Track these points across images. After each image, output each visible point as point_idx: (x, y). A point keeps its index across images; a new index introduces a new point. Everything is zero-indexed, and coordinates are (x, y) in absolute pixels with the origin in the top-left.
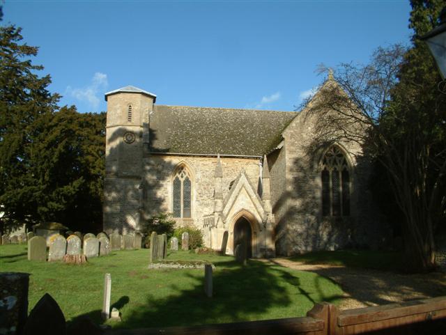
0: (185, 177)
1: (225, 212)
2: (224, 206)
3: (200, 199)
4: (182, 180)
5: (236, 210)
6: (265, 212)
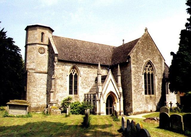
0: (75, 73)
1: (103, 93)
2: (103, 90)
3: (82, 85)
4: (74, 75)
5: (108, 92)
6: (120, 93)
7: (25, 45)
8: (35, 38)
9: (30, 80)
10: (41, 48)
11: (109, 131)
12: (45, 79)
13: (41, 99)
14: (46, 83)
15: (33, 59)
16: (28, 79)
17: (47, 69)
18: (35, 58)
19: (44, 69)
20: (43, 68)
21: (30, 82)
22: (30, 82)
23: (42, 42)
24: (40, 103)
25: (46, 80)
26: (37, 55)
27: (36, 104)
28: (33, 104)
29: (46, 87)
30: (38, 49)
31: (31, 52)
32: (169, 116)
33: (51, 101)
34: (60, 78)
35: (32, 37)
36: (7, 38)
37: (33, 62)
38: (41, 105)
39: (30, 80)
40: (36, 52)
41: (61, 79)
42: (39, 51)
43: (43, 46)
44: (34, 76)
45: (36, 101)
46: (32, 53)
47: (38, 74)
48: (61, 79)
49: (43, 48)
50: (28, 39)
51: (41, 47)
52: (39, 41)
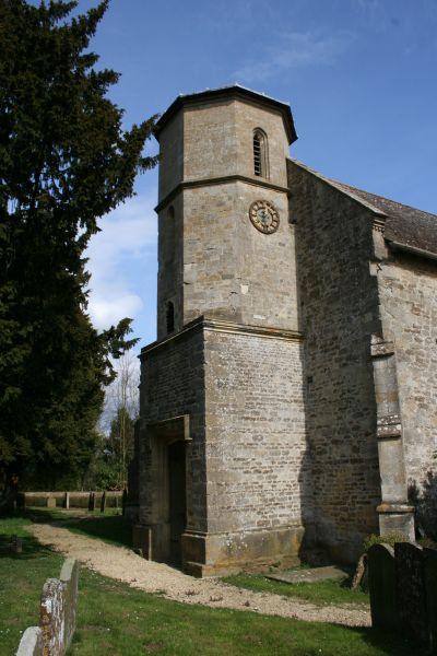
7: (156, 205)
8: (223, 151)
9: (217, 372)
10: (260, 203)
11: (207, 599)
12: (290, 370)
13: (281, 486)
14: (299, 395)
15: (223, 259)
16: (209, 366)
17: (295, 314)
18: (235, 253)
19: (283, 314)
20: (275, 309)
21: (219, 385)
22: (219, 385)
23: (257, 174)
24: (278, 512)
25: (298, 378)
26: (245, 238)
27: (259, 518)
28: (241, 517)
29: (302, 416)
30: (248, 207)
31: (209, 222)
32: (392, 551)
33: (385, 496)
34: (409, 352)
35: (205, 150)
36: (105, 97)
37: (225, 277)
38: (283, 520)
39: (217, 372)
40: (236, 220)
41: (413, 358)
42: (251, 216)
43: (267, 194)
44: (237, 353)
45: (255, 500)
46: (214, 226)
47: (255, 342)
48: (413, 358)
49: (268, 205)
50: (186, 159)
51: (259, 198)
52: (247, 169)
